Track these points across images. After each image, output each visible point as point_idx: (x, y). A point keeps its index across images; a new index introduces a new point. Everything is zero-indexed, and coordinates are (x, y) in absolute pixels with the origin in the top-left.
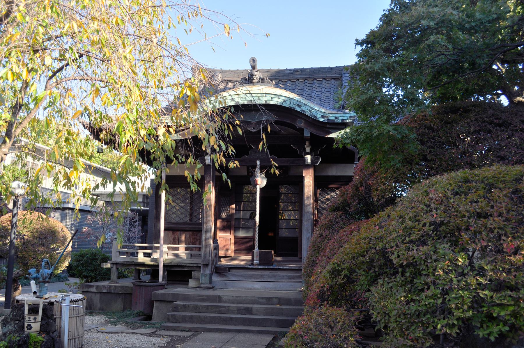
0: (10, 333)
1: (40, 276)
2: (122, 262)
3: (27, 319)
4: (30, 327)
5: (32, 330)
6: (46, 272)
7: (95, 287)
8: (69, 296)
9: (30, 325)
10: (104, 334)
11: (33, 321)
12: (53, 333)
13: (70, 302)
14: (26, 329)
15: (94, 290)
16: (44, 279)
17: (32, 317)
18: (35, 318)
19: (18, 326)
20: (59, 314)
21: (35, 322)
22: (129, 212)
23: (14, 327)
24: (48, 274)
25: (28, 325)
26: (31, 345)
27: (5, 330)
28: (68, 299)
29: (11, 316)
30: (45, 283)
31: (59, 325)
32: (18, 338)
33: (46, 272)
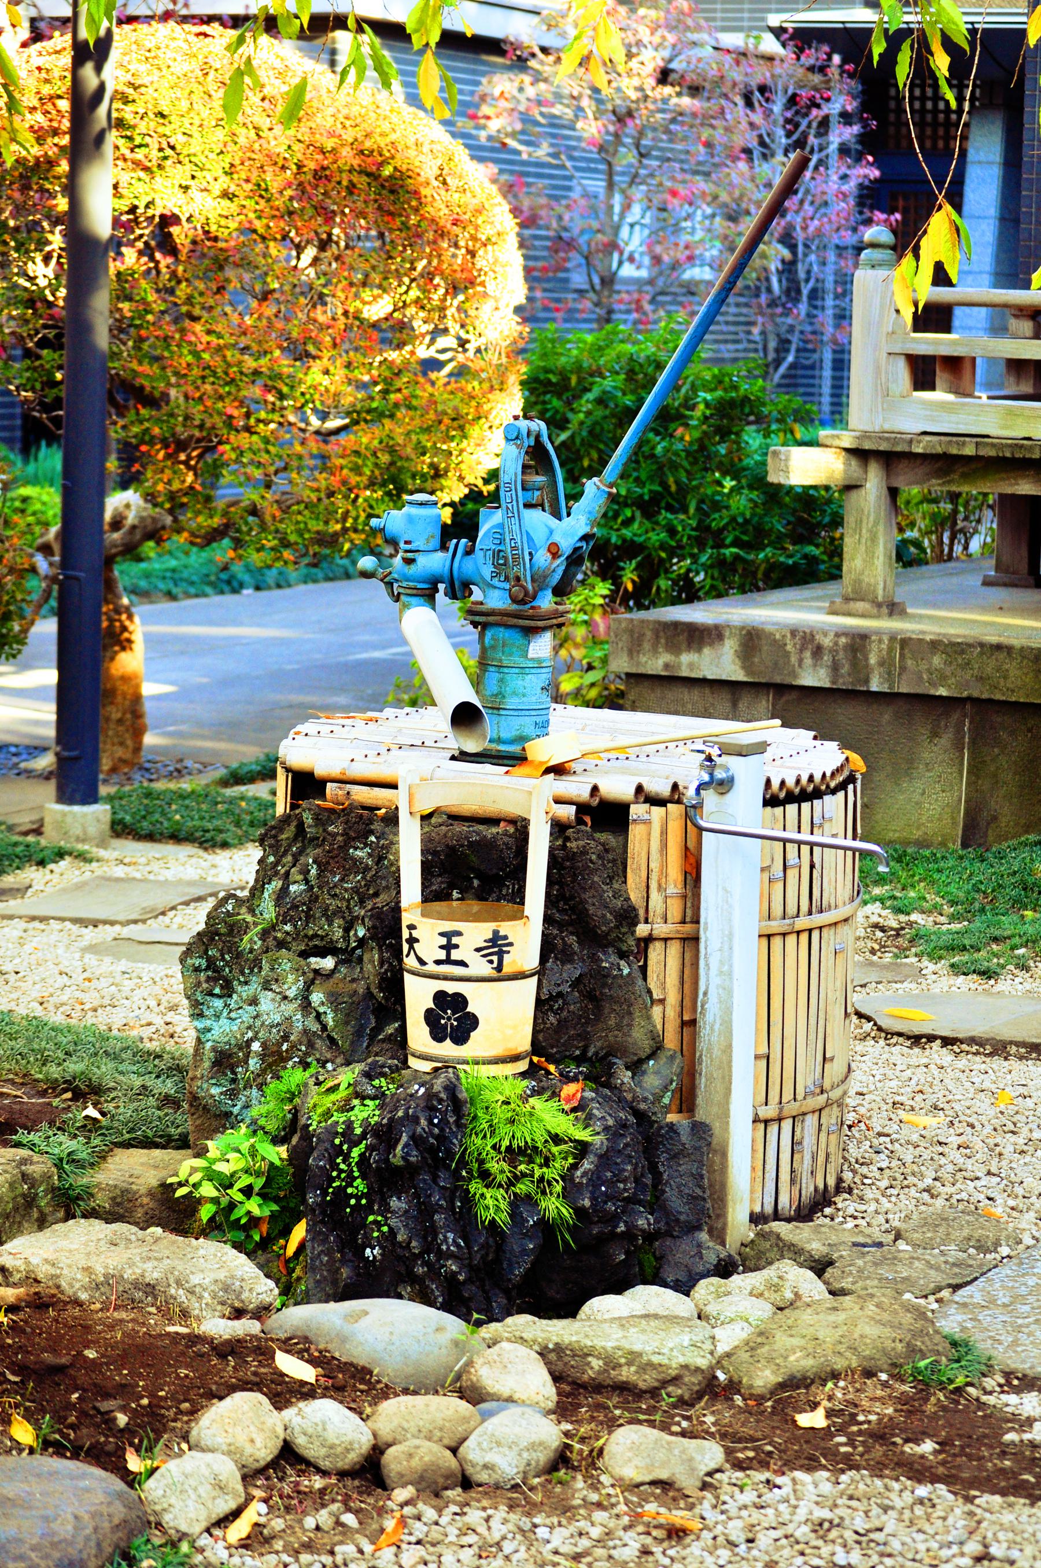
0: (275, 1060)
1: (480, 565)
2: (936, 446)
3: (429, 947)
4: (453, 1018)
5: (478, 1045)
6: (540, 538)
7: (729, 648)
8: (760, 748)
9: (459, 1002)
10: (937, 1053)
11: (480, 967)
12: (636, 1066)
13: (771, 801)
14: (418, 1035)
15: (722, 663)
16: (524, 599)
17: (474, 934)
18: (497, 946)
19: (333, 999)
20: (675, 911)
21: (500, 976)
22: (770, 45)
23: (306, 1006)
24: (554, 551)
25: (440, 997)
26: (485, 1175)
27: (223, 1031)
28: (749, 777)
29: (268, 910)
30: (531, 632)
31: (673, 998)
32: (365, 1113)
33: (540, 538)
